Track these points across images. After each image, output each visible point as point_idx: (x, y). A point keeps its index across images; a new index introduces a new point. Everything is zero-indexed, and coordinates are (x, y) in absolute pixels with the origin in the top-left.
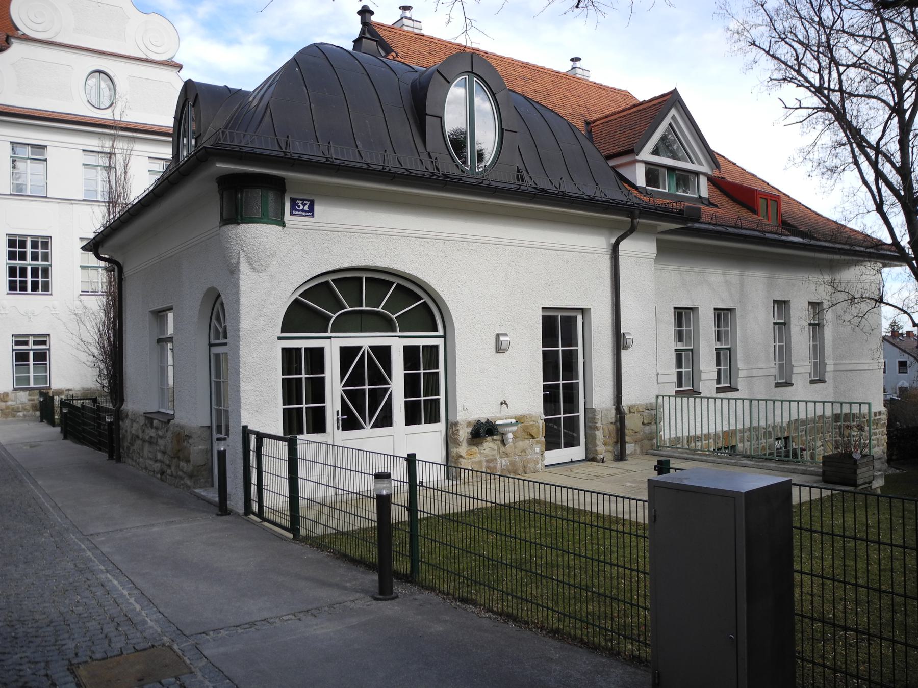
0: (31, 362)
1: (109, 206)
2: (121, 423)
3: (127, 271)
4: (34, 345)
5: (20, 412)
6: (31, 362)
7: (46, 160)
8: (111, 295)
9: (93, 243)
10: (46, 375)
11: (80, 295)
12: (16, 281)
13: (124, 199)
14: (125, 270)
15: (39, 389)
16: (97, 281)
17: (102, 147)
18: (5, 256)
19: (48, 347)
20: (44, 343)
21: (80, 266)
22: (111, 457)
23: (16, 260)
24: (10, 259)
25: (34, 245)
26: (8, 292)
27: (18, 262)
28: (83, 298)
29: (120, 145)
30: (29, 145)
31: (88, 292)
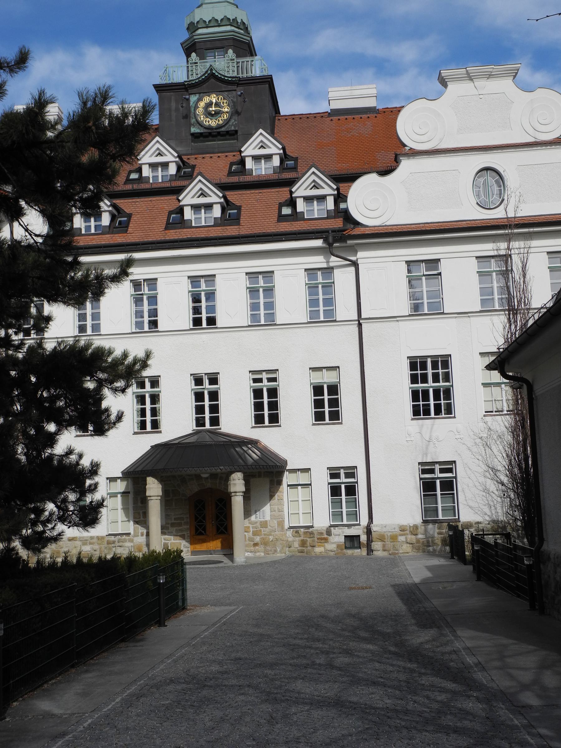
0: (439, 492)
1: (509, 314)
2: (542, 566)
3: (538, 390)
4: (440, 473)
5: (430, 546)
6: (439, 492)
7: (440, 274)
8: (517, 414)
9: (498, 361)
10: (454, 506)
11: (484, 416)
12: (420, 405)
13: (525, 305)
14: (536, 387)
15: (448, 521)
16: (501, 399)
17: (497, 250)
18: (407, 380)
19: (454, 475)
20: (450, 470)
21: (482, 384)
22: (532, 607)
23: (418, 383)
24: (412, 383)
25: (435, 365)
26: (413, 417)
27: (420, 385)
28: (489, 419)
29: (515, 244)
30: (422, 261)
31: (492, 412)
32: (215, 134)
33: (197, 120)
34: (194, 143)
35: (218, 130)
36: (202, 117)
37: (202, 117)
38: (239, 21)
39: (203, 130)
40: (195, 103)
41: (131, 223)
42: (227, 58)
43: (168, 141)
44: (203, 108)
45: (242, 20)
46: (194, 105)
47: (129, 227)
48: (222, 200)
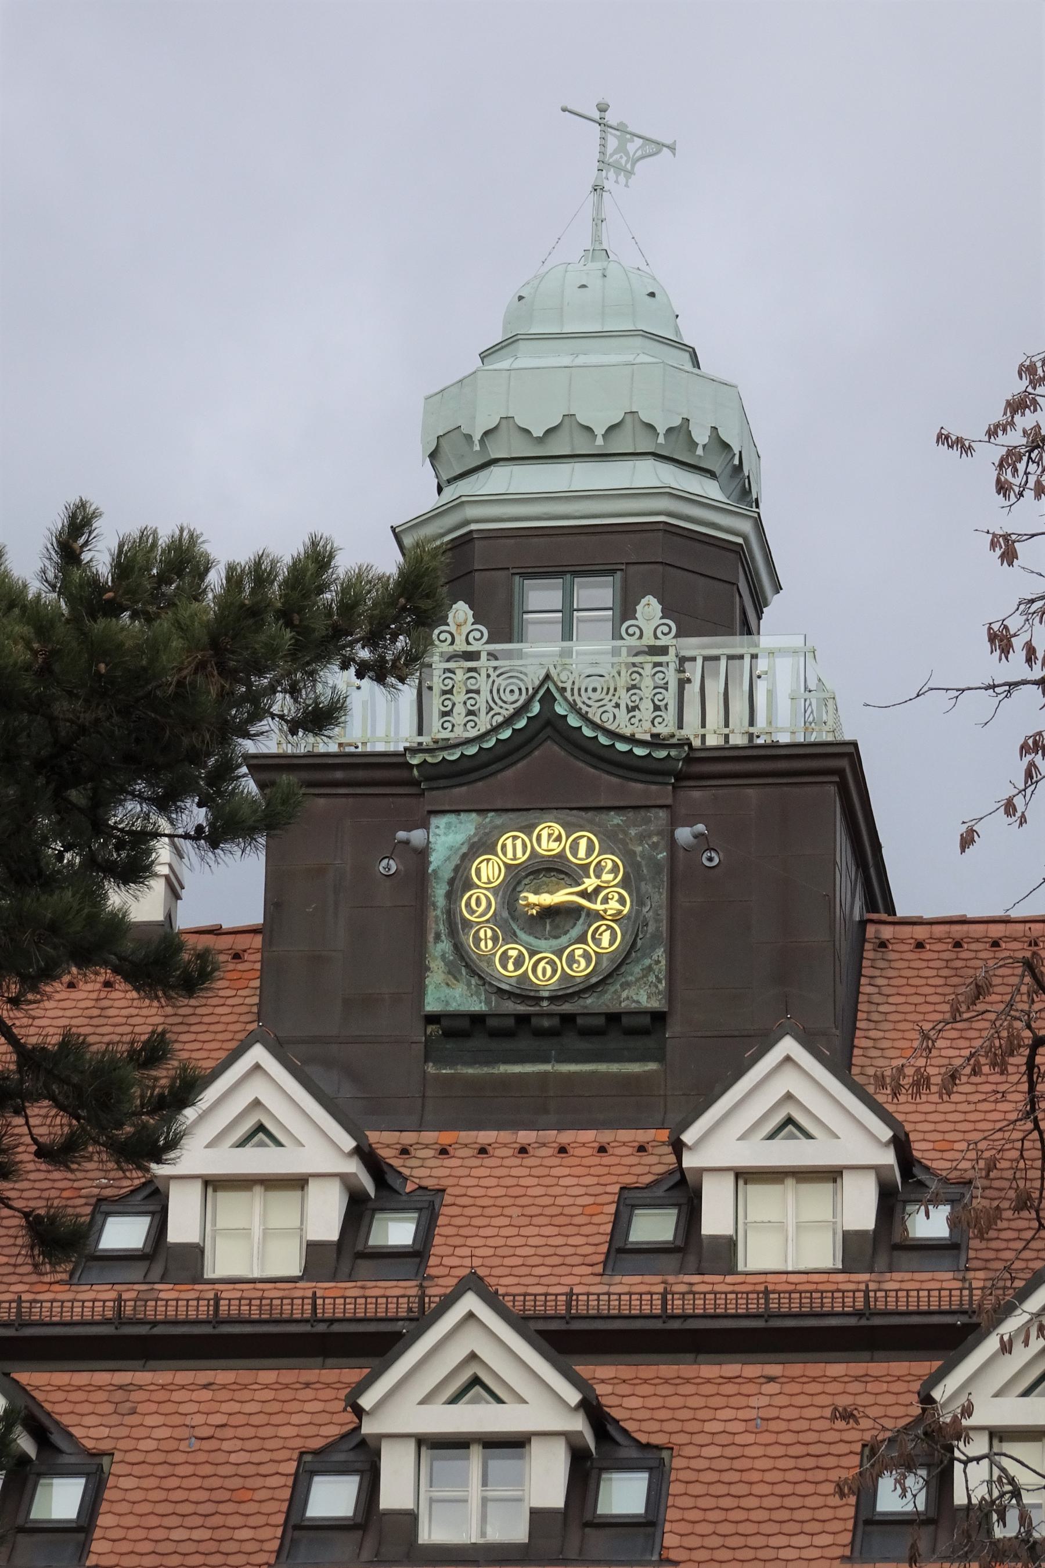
32: (546, 1023)
33: (458, 948)
34: (440, 1061)
35: (567, 1008)
36: (485, 933)
37: (485, 933)
38: (701, 437)
39: (488, 1002)
40: (456, 860)
41: (104, 1507)
42: (632, 642)
43: (306, 1069)
44: (495, 891)
45: (714, 429)
46: (447, 874)
47: (98, 1533)
48: (578, 1424)
